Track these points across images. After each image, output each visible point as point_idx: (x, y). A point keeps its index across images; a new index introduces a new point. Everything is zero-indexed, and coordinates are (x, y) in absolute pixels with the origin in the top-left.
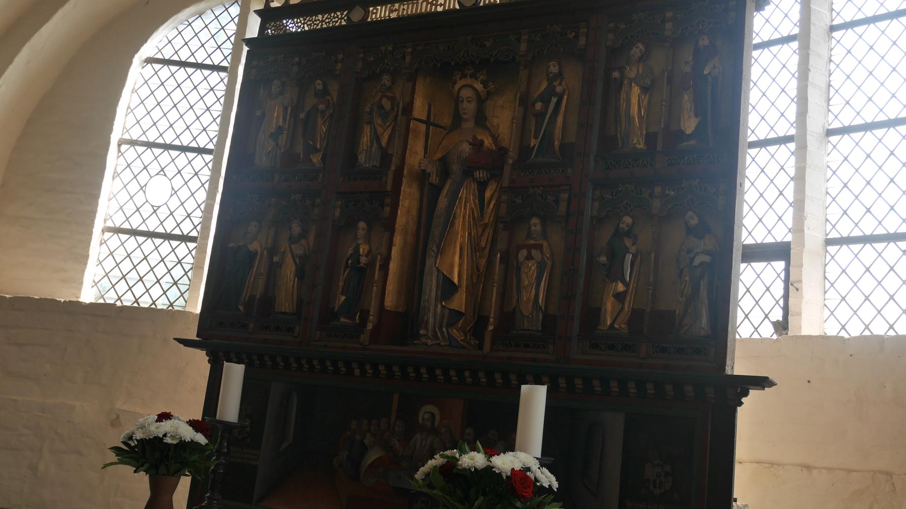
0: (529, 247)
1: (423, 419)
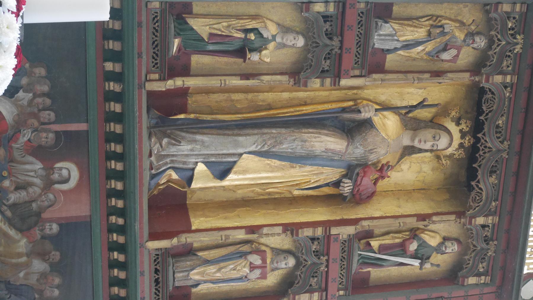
0: (263, 267)
1: (61, 169)
